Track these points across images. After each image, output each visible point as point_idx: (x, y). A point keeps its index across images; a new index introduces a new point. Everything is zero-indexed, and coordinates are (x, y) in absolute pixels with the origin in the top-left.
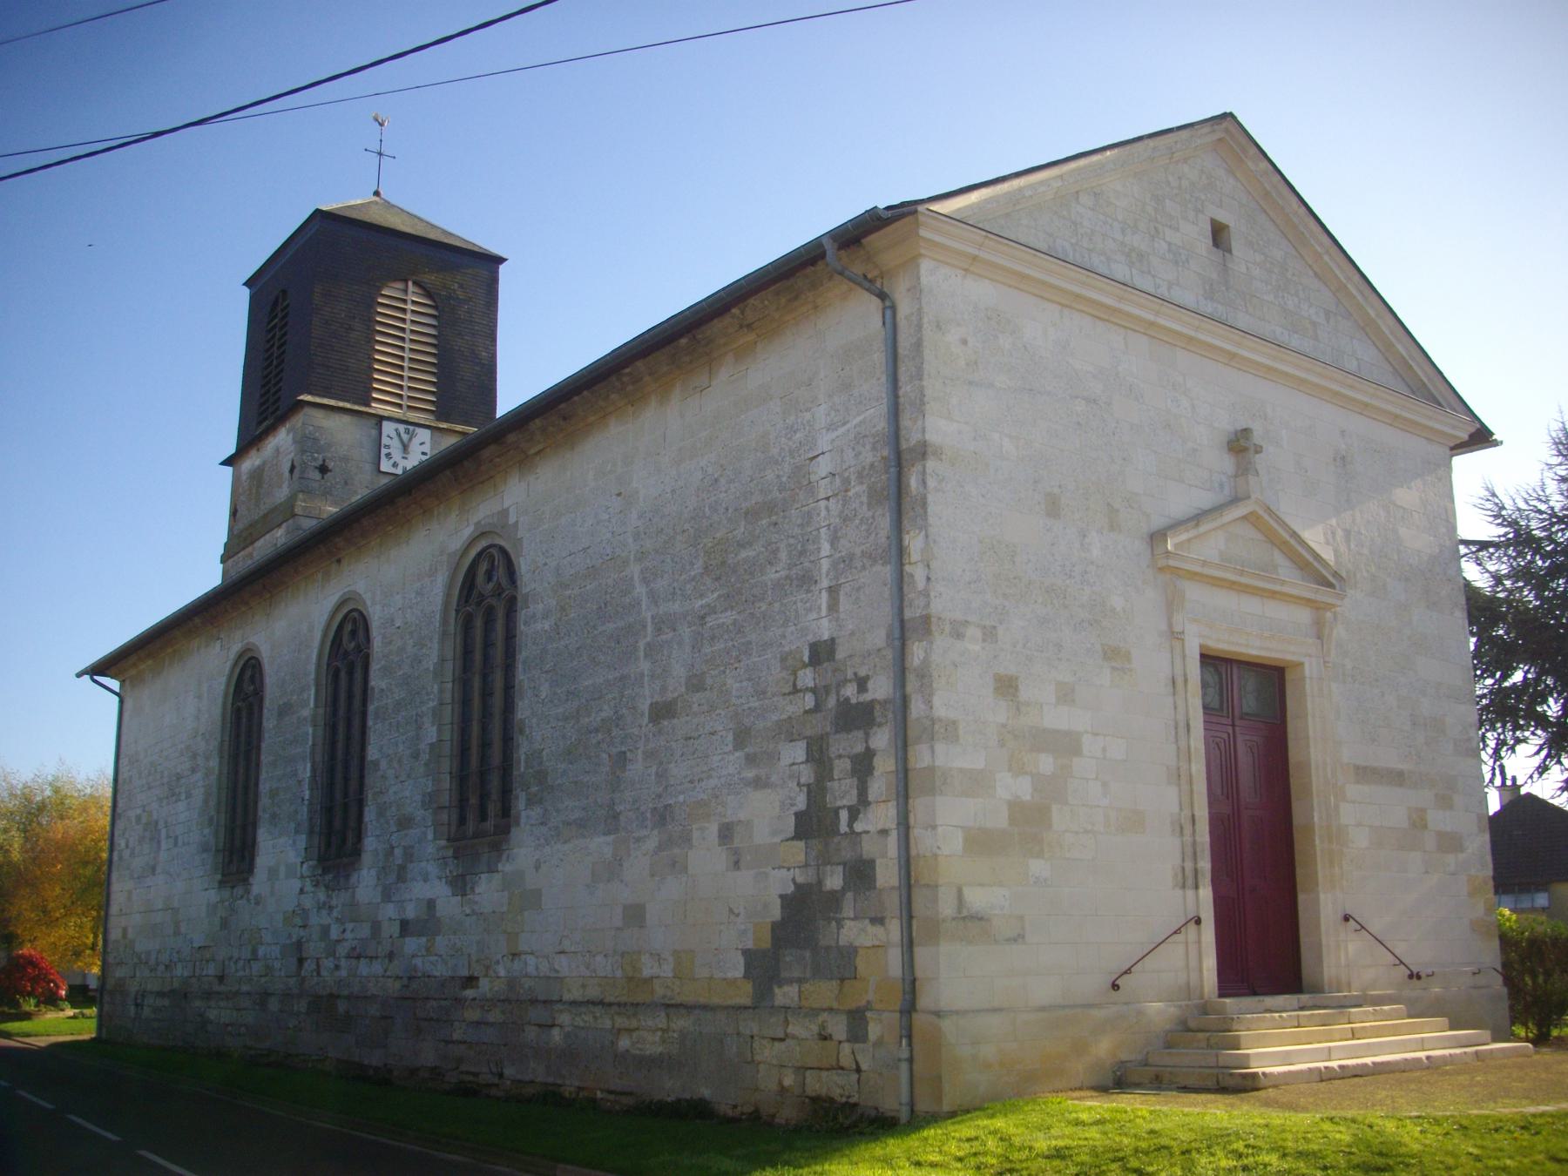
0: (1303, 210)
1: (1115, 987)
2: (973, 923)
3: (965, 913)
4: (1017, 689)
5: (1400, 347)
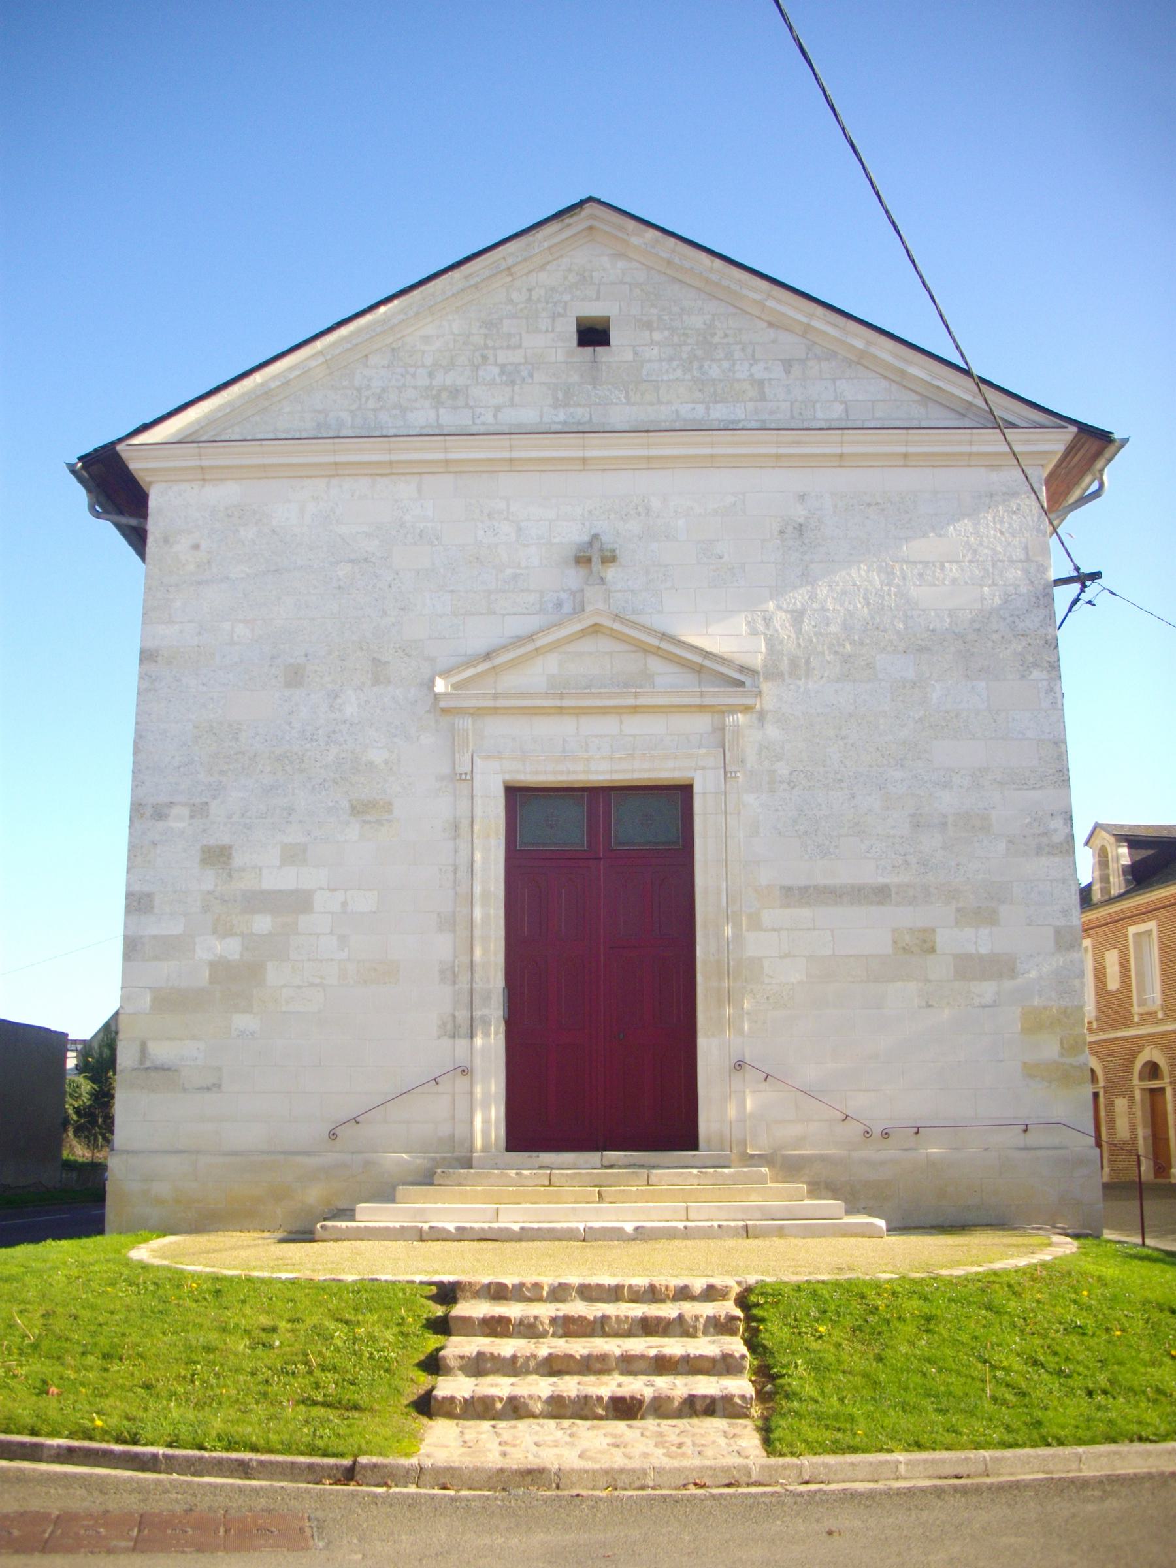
0: (718, 263)
1: (333, 1135)
2: (161, 1074)
3: (148, 1064)
4: (229, 857)
5: (913, 370)
